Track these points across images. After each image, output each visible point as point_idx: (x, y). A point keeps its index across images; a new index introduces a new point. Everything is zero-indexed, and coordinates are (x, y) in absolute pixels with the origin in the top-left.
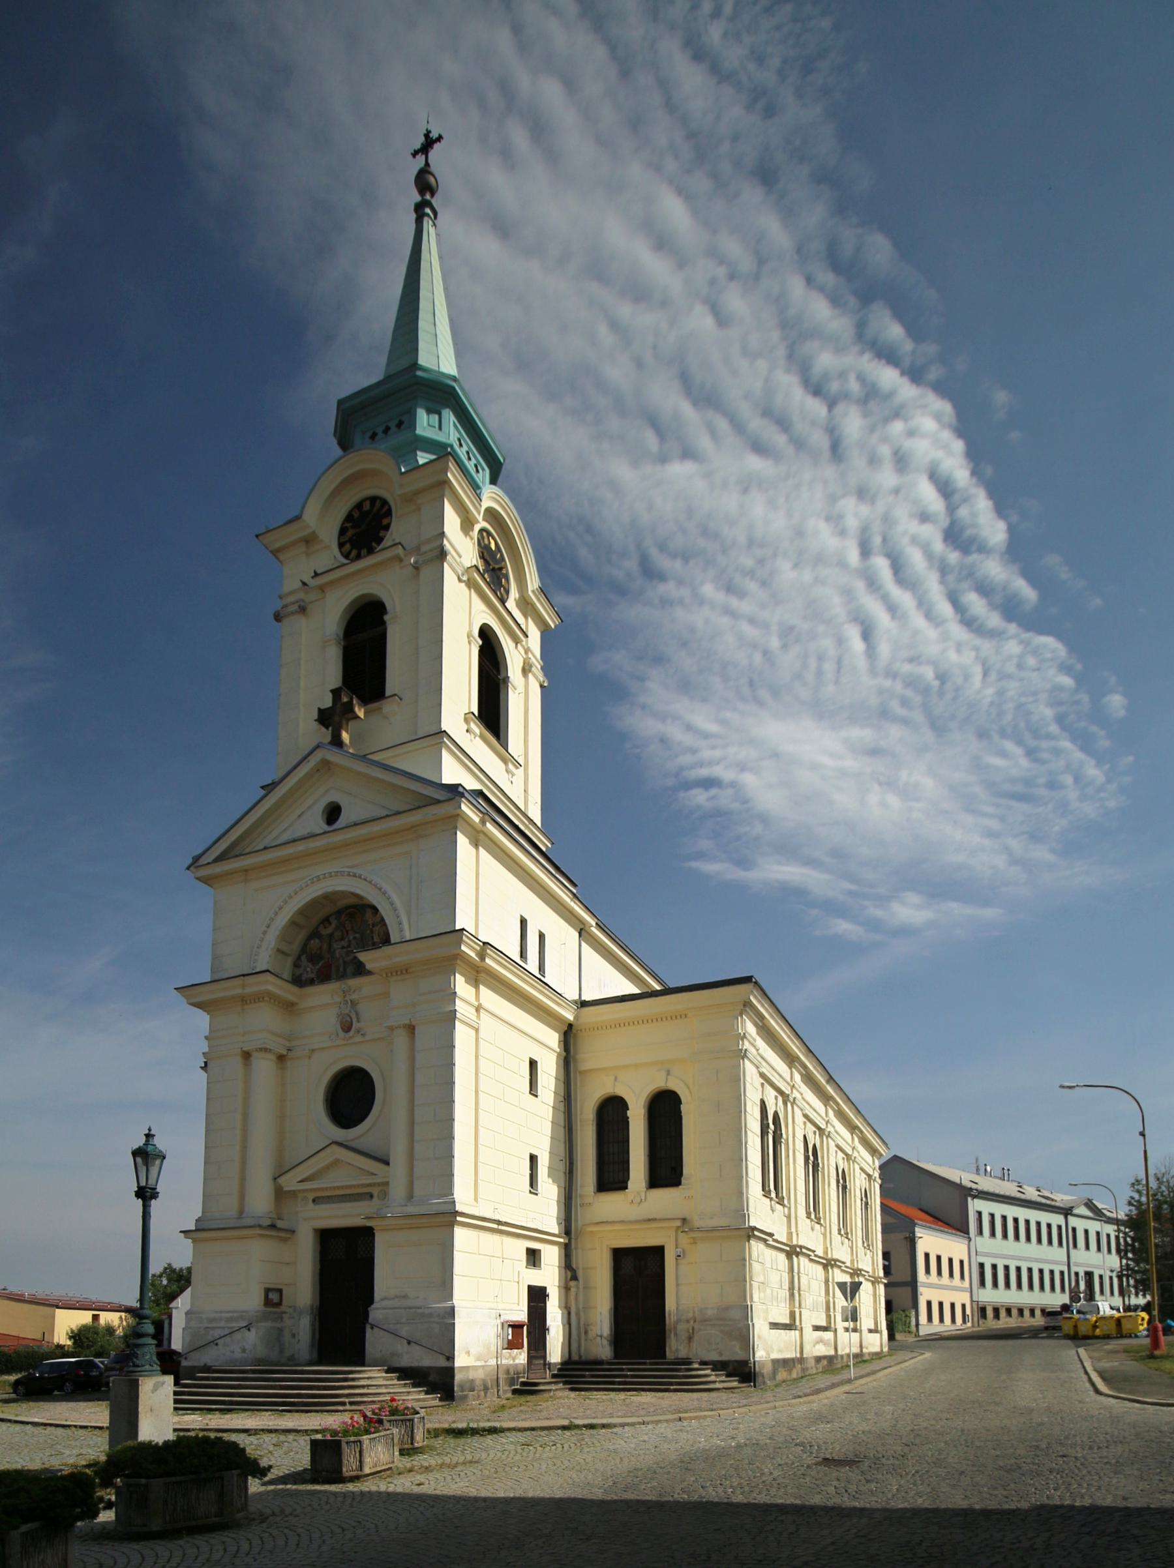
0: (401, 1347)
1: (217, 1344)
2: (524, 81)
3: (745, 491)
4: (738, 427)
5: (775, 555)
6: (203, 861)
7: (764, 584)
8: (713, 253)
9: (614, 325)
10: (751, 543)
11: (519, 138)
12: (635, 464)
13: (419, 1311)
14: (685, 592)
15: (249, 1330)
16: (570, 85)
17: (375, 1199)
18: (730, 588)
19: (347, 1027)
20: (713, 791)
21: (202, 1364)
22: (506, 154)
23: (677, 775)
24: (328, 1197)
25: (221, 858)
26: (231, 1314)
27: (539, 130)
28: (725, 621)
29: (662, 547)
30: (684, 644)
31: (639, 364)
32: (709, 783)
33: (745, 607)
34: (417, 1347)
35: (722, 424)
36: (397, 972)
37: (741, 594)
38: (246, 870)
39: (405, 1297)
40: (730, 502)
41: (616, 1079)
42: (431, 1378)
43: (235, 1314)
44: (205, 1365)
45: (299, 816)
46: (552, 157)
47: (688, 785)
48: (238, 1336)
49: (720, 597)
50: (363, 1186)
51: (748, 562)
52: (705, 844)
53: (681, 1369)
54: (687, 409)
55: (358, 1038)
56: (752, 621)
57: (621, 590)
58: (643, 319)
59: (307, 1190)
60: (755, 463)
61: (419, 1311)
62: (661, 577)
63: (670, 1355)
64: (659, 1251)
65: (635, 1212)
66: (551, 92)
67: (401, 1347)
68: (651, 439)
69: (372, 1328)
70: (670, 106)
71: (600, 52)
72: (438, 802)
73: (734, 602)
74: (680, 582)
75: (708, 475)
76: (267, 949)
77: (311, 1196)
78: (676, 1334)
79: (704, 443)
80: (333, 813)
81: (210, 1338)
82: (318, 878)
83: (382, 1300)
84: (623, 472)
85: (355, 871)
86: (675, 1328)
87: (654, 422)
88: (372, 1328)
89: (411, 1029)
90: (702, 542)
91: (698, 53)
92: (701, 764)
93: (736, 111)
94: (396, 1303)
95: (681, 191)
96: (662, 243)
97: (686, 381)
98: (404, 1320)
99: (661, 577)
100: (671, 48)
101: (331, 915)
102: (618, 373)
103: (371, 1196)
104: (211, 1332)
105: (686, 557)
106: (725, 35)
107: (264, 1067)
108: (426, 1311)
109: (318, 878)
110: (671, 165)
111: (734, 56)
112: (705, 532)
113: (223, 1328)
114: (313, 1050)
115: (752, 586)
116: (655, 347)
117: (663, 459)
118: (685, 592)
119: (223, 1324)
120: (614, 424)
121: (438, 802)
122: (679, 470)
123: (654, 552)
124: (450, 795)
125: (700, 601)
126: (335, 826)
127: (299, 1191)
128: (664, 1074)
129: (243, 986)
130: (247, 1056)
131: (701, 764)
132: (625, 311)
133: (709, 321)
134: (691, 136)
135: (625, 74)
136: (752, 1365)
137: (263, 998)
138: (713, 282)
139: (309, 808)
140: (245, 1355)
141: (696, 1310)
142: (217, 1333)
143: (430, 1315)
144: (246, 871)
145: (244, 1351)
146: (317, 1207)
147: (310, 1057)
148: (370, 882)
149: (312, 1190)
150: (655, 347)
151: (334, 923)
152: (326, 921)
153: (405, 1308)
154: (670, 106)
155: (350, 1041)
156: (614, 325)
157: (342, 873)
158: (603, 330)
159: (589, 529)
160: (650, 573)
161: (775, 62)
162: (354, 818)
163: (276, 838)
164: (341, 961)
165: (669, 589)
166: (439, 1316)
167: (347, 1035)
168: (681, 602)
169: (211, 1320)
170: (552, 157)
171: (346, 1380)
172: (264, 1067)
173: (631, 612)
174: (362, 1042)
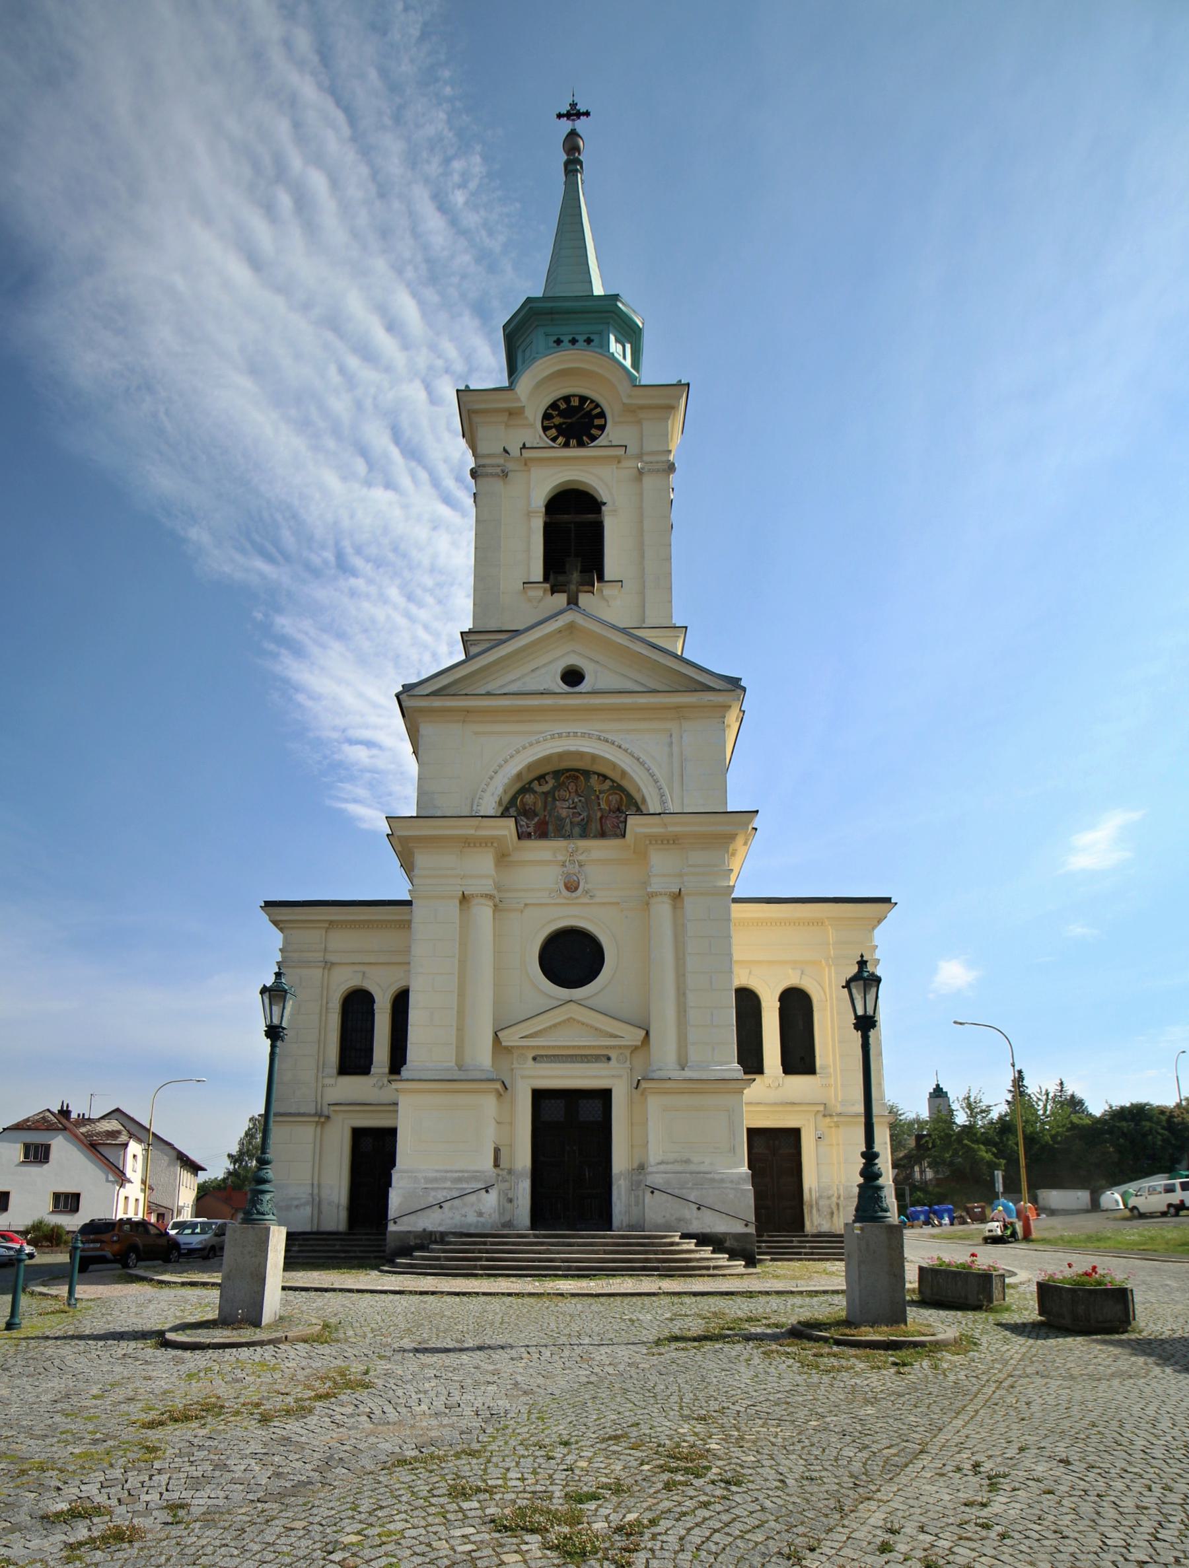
0: (689, 1212)
1: (441, 1207)
2: (296, 163)
3: (435, 528)
4: (436, 482)
5: (452, 585)
6: (417, 691)
7: (440, 602)
8: (433, 348)
9: (342, 370)
10: (432, 570)
11: (285, 201)
12: (344, 479)
13: (709, 1176)
14: (373, 590)
15: (487, 1191)
16: (335, 183)
17: (613, 1062)
18: (410, 597)
19: (572, 887)
20: (374, 751)
21: (421, 1230)
22: (269, 210)
23: (344, 731)
24: (554, 1056)
25: (434, 694)
26: (460, 1175)
27: (303, 202)
28: (401, 621)
29: (359, 550)
30: (366, 631)
31: (359, 406)
32: (369, 744)
33: (423, 614)
34: (709, 1212)
35: (423, 475)
36: (480, 844)
37: (421, 605)
38: (468, 711)
39: (688, 1161)
40: (421, 533)
41: (750, 973)
42: (727, 1244)
43: (466, 1175)
44: (424, 1230)
45: (532, 671)
46: (311, 229)
47: (352, 742)
48: (473, 1198)
49: (401, 601)
50: (600, 1047)
51: (429, 582)
52: (362, 792)
53: (440, 1257)
54: (395, 452)
55: (586, 900)
56: (426, 627)
57: (316, 572)
58: (367, 374)
59: (528, 1047)
60: (444, 510)
61: (709, 1176)
62: (354, 573)
63: (809, 1227)
64: (795, 1133)
65: (772, 1096)
66: (318, 181)
67: (689, 1212)
68: (360, 466)
69: (652, 1192)
70: (416, 234)
71: (364, 171)
72: (713, 690)
73: (413, 609)
74: (370, 581)
75: (406, 507)
76: (493, 794)
77: (531, 1055)
78: (818, 1210)
79: (406, 482)
80: (573, 677)
81: (431, 1200)
82: (560, 735)
83: (659, 1164)
84: (331, 480)
85: (607, 736)
86: (817, 1203)
87: (363, 451)
88: (652, 1192)
89: (677, 897)
90: (391, 556)
91: (443, 206)
92: (367, 726)
93: (466, 258)
94: (678, 1167)
95: (415, 295)
96: (392, 327)
97: (397, 435)
98: (690, 1185)
99: (354, 573)
100: (422, 197)
101: (548, 773)
102: (340, 406)
103: (609, 1059)
104: (433, 1193)
105: (379, 563)
106: (466, 203)
107: (484, 913)
108: (717, 1177)
109: (560, 735)
110: (410, 274)
111: (471, 219)
112: (395, 550)
113: (450, 1189)
114: (526, 905)
115: (430, 600)
116: (375, 398)
117: (368, 484)
118: (373, 590)
119: (448, 1184)
120: (331, 444)
121: (713, 690)
122: (380, 495)
123: (349, 550)
124: (730, 687)
125: (384, 600)
126: (577, 689)
127: (518, 1047)
128: (799, 972)
129: (477, 828)
130: (464, 899)
131: (367, 726)
132: (353, 362)
133: (422, 395)
134: (428, 261)
135: (382, 195)
136: (141, 1273)
137: (492, 843)
138: (431, 368)
139: (544, 665)
140: (482, 1219)
141: (841, 1188)
142: (441, 1196)
143: (722, 1180)
144: (468, 712)
145: (480, 1214)
146: (538, 1065)
147: (522, 912)
148: (626, 750)
149: (533, 1047)
150: (375, 398)
151: (551, 783)
152: (541, 778)
153: (691, 1173)
154: (416, 234)
155: (577, 901)
156: (342, 370)
157: (590, 736)
158: (333, 370)
159: (295, 516)
160: (343, 566)
161: (502, 238)
162: (601, 685)
163: (502, 686)
164: (568, 820)
165: (358, 583)
166: (732, 1182)
167: (574, 895)
168: (368, 596)
169: (428, 1180)
170: (311, 229)
171: (653, 1244)
172: (484, 913)
173: (321, 593)
174: (588, 904)
